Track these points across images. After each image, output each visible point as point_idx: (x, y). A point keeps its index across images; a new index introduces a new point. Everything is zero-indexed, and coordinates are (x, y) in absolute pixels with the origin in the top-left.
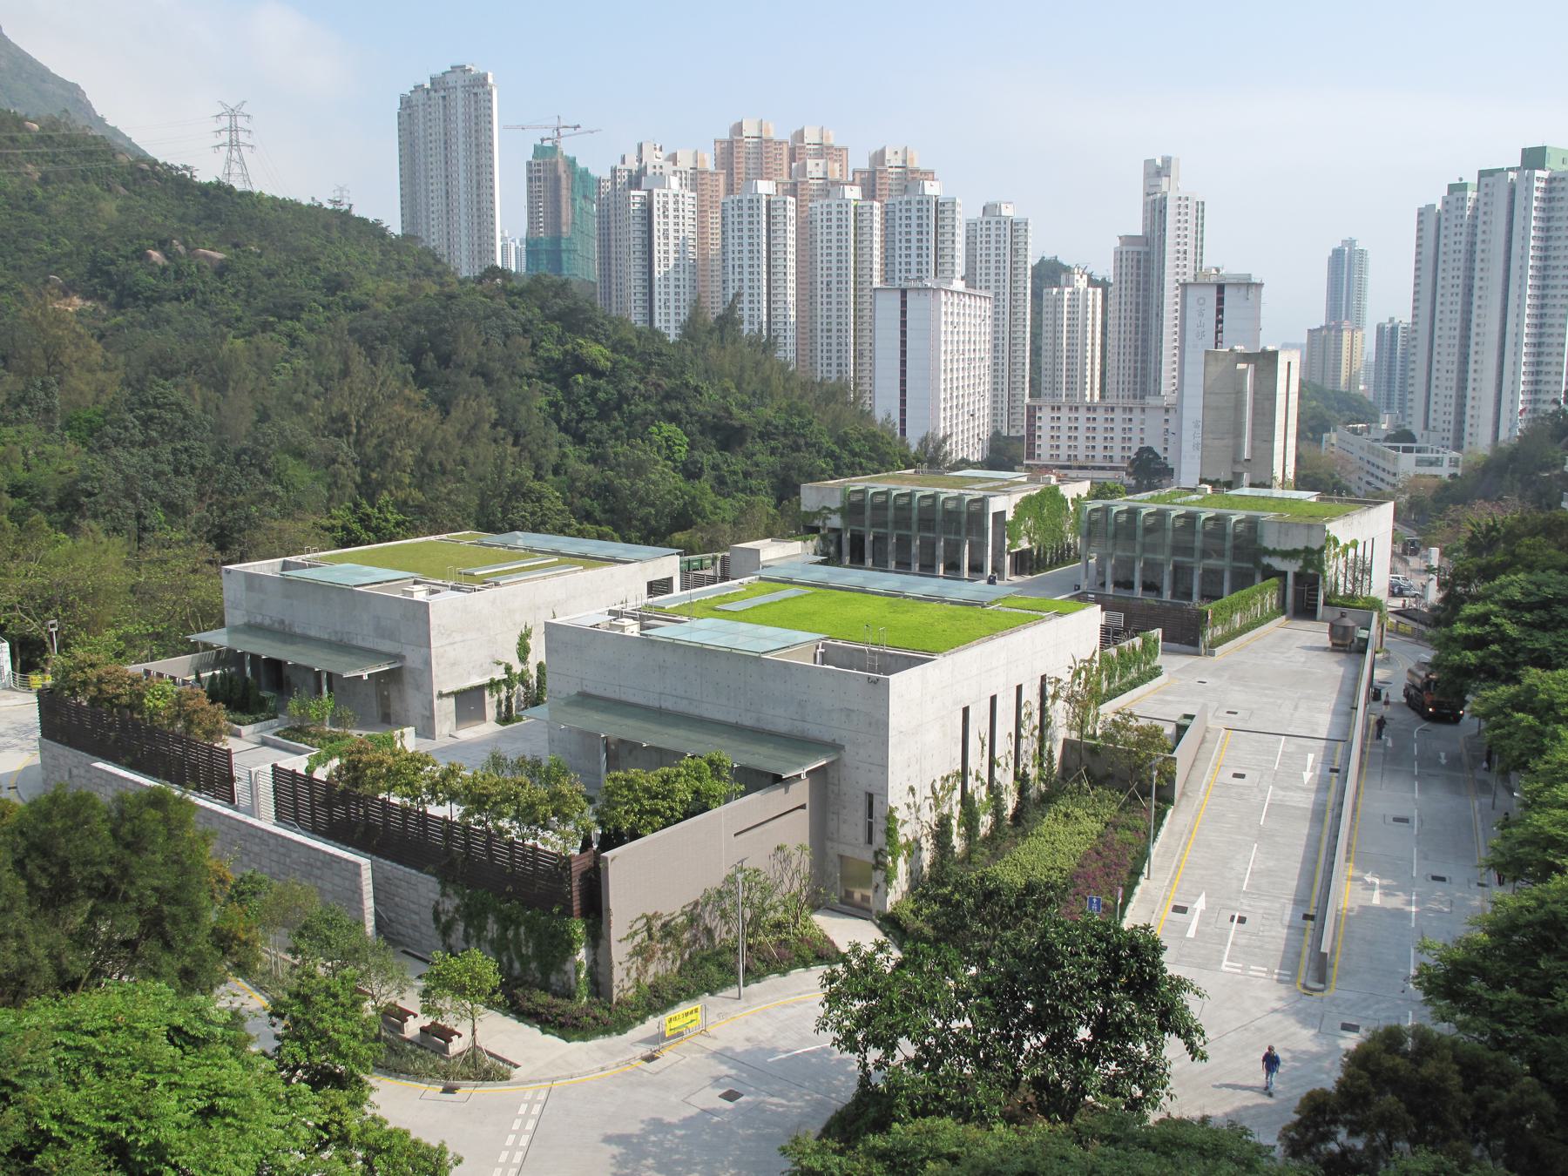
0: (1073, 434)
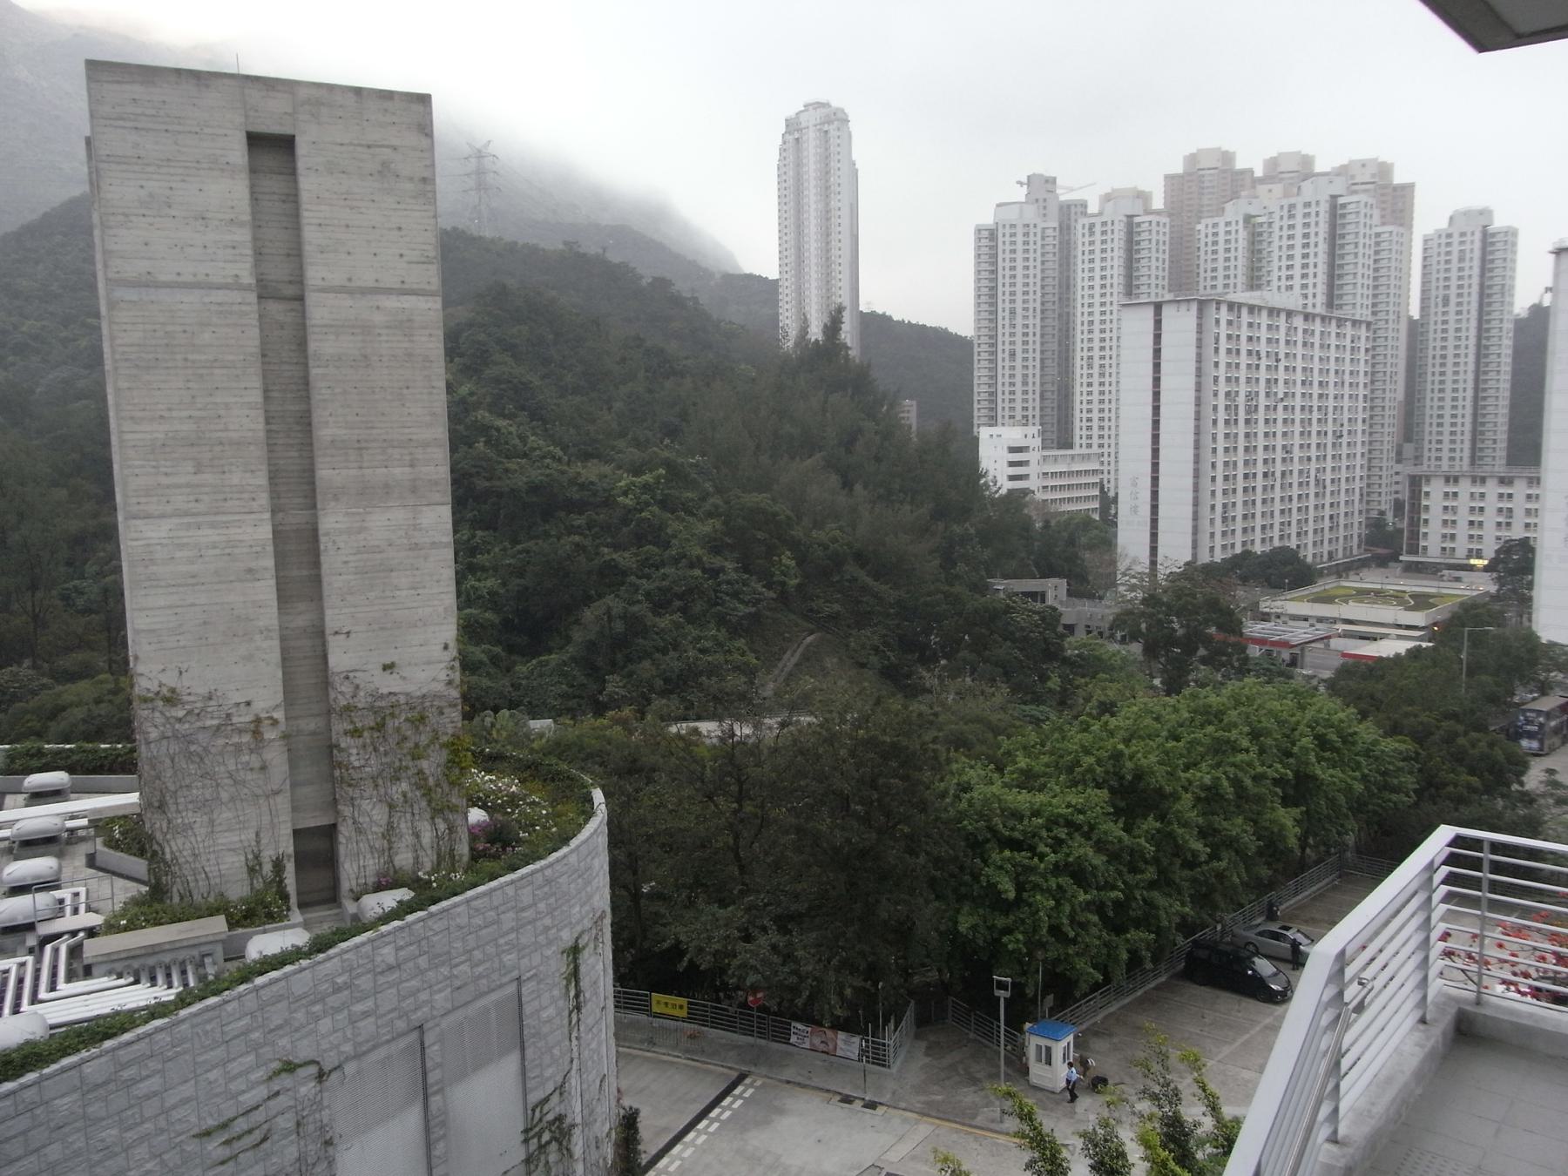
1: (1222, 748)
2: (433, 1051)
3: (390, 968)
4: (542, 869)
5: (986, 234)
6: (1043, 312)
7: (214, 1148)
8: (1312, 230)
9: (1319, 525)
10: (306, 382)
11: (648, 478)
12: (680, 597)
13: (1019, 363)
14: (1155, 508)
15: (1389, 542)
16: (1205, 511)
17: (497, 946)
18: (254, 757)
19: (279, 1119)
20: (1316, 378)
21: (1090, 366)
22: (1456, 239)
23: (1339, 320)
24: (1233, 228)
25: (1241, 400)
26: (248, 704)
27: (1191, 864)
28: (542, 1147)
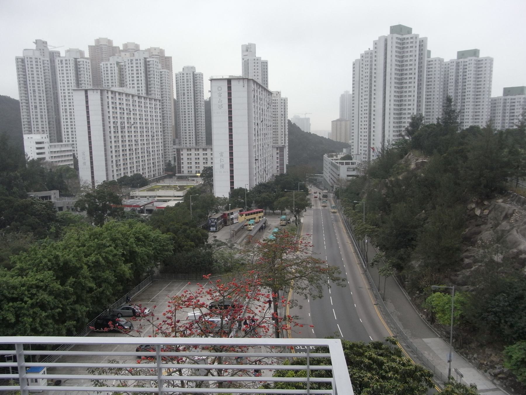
0: (197, 161)
1: (101, 247)
5: (20, 60)
6: (46, 91)
8: (139, 68)
9: (149, 166)
13: (38, 110)
14: (92, 163)
15: (172, 170)
16: (110, 163)
20: (144, 118)
21: (66, 112)
22: (185, 75)
23: (150, 99)
24: (113, 66)
25: (119, 124)
27: (91, 290)
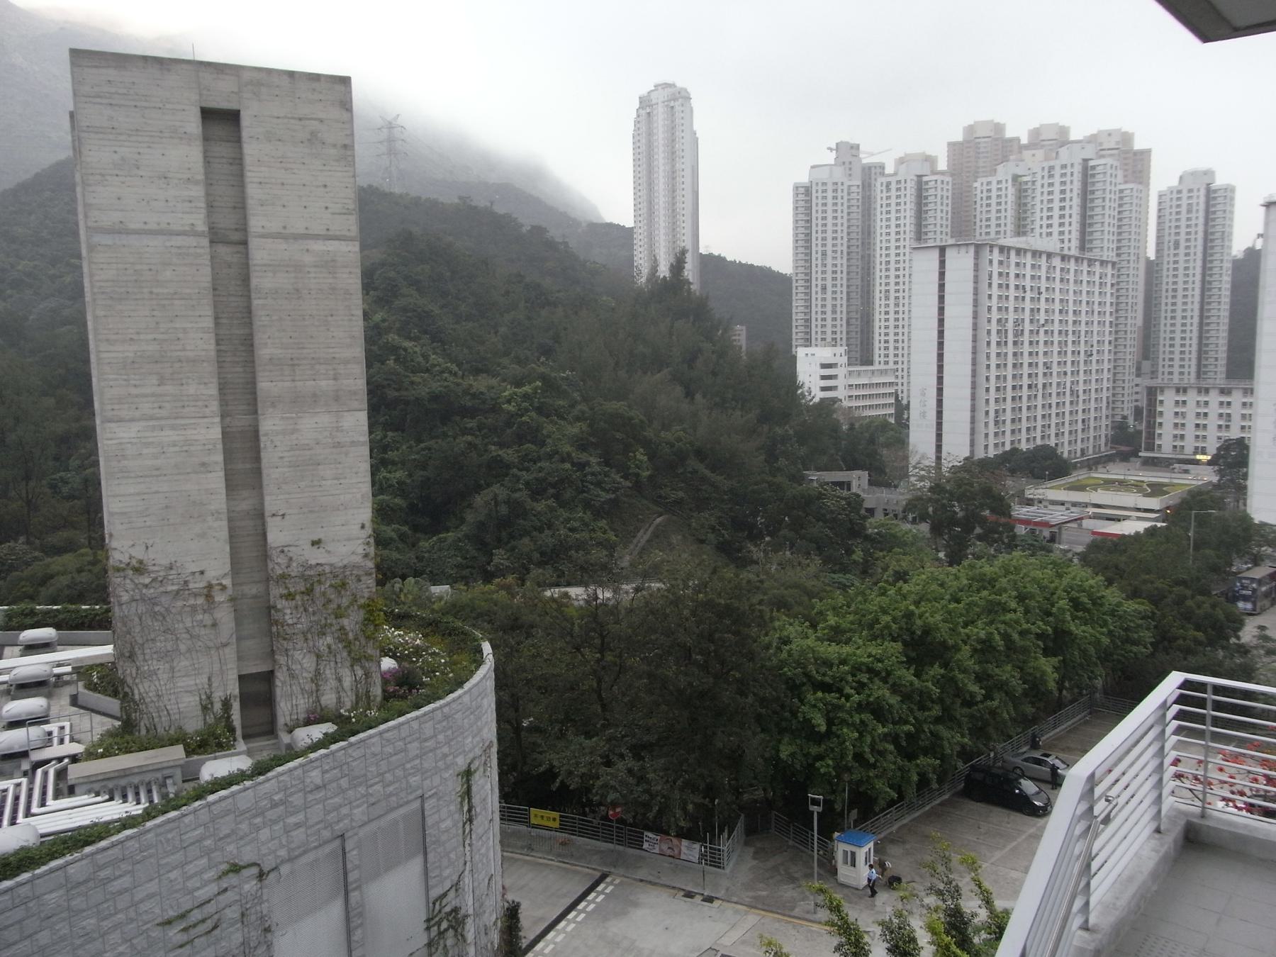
1: (995, 609)
2: (352, 855)
3: (318, 788)
4: (441, 707)
5: (802, 190)
6: (848, 254)
7: (174, 934)
8: (1068, 187)
9: (1073, 427)
10: (249, 311)
11: (527, 389)
12: (553, 486)
13: (829, 295)
14: (940, 414)
15: (1130, 441)
16: (981, 416)
17: (405, 770)
18: (207, 616)
19: (227, 911)
20: (1071, 308)
21: (887, 298)
22: (1185, 195)
23: (1090, 260)
24: (1003, 185)
25: (1010, 325)
26: (202, 573)
27: (969, 703)
28: (441, 934)
